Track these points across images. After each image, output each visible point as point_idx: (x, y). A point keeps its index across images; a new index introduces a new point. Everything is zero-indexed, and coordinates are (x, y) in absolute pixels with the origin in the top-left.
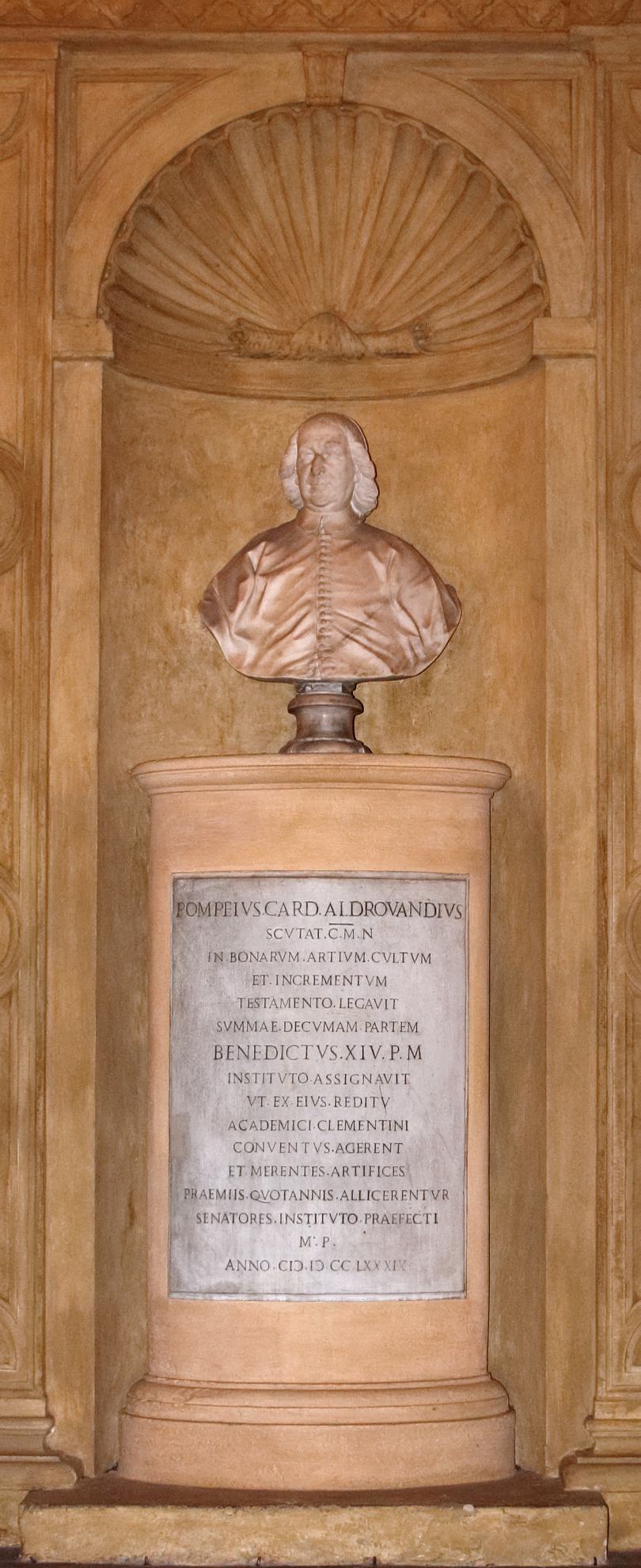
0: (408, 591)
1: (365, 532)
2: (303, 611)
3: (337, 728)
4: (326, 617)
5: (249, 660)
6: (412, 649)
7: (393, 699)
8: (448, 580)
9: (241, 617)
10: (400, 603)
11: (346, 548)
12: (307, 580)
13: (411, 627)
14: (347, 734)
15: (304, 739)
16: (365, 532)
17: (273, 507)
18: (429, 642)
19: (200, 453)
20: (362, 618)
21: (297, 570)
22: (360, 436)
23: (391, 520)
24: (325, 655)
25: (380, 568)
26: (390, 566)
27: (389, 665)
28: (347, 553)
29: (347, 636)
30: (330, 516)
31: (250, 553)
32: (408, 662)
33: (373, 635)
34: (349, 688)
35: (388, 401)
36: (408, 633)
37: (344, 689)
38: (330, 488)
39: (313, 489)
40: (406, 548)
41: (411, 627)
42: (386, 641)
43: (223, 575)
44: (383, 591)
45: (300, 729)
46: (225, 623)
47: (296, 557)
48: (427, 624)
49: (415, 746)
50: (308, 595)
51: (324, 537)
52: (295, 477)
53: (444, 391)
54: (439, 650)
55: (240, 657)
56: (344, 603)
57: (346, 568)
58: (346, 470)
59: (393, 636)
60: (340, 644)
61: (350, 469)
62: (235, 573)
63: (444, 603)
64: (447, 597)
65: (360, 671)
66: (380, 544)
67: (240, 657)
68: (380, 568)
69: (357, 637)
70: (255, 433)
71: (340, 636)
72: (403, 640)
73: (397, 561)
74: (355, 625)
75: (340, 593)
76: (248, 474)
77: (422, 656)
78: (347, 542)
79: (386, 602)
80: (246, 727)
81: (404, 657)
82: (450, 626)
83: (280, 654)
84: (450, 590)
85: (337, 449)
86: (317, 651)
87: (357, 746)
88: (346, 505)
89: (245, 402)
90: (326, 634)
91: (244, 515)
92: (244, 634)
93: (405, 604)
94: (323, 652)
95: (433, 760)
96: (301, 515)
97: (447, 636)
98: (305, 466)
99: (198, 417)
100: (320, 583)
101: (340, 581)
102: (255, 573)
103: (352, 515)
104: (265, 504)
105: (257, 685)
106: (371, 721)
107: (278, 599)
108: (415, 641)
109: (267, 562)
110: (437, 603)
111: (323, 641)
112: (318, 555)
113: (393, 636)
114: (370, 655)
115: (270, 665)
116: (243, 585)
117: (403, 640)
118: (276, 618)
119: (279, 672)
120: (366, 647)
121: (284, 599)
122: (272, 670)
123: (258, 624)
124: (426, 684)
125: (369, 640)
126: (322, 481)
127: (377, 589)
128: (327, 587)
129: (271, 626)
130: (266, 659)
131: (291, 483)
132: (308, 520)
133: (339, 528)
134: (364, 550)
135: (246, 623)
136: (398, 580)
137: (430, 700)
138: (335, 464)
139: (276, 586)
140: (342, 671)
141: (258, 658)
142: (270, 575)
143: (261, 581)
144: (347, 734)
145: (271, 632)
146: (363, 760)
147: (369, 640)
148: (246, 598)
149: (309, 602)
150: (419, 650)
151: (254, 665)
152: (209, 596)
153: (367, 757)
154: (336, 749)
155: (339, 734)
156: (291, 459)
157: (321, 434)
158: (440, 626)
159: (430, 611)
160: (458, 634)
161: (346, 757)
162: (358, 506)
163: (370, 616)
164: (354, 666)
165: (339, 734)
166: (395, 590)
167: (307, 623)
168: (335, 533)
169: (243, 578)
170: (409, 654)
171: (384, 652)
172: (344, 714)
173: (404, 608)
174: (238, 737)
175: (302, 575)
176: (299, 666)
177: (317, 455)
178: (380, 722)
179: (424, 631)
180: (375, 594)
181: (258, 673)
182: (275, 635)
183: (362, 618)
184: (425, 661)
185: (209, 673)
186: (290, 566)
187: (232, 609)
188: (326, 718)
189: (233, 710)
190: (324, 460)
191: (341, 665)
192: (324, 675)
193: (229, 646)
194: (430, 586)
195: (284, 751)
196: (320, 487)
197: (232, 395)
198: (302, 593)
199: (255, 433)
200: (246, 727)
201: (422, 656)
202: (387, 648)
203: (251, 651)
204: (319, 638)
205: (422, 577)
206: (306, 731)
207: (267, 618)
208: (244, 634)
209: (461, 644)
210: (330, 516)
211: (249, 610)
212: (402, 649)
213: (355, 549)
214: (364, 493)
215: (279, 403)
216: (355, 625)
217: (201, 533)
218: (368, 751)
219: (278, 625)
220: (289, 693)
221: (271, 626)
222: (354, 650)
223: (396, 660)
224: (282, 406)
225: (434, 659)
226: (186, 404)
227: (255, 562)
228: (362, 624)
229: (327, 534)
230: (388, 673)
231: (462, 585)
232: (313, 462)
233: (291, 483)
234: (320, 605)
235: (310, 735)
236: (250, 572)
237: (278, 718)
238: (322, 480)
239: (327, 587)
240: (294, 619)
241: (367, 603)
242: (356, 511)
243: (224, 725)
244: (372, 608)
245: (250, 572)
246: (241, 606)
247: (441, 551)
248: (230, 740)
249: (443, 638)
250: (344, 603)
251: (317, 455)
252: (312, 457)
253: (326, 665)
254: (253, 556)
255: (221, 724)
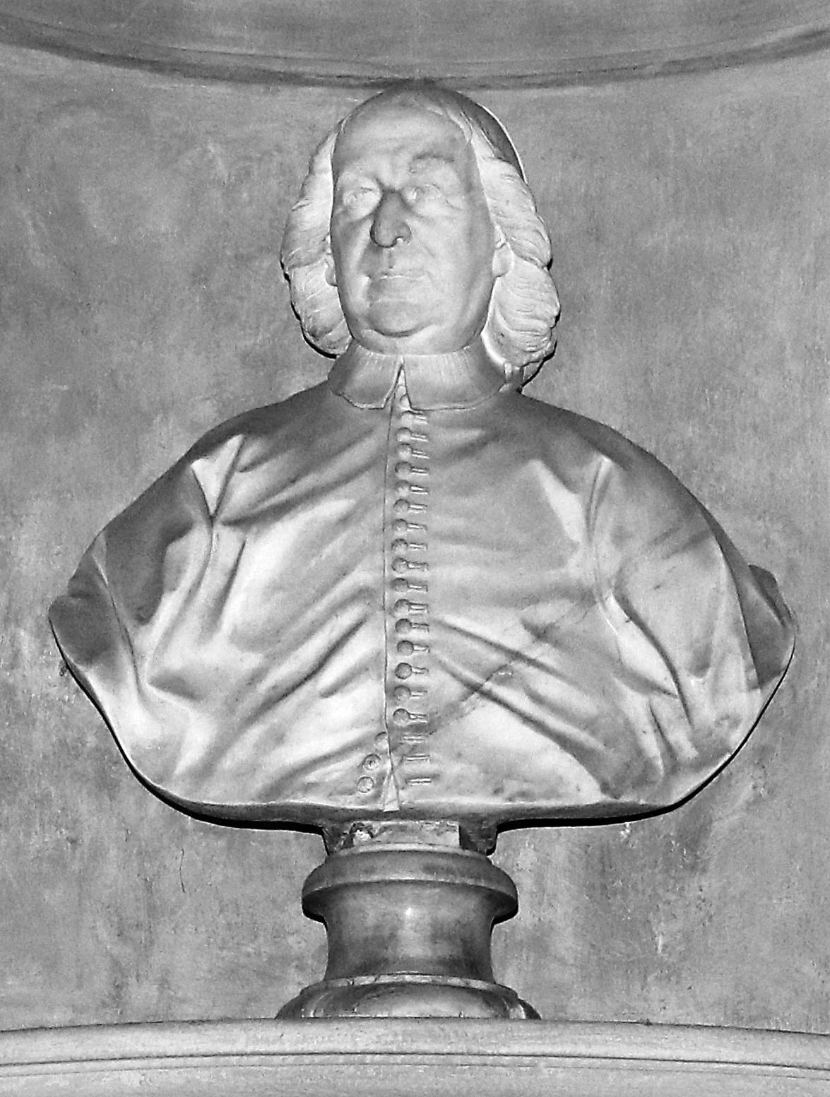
0: (646, 571)
1: (521, 415)
2: (346, 619)
3: (444, 950)
4: (414, 635)
5: (191, 756)
6: (659, 729)
7: (601, 878)
8: (752, 554)
9: (170, 637)
10: (624, 602)
11: (467, 451)
12: (361, 533)
13: (655, 669)
14: (467, 965)
15: (351, 980)
16: (521, 415)
17: (266, 363)
18: (706, 713)
19: (68, 217)
20: (517, 639)
21: (331, 507)
22: (326, 927)
23: (590, 387)
24: (412, 740)
25: (566, 506)
26: (595, 498)
27: (594, 771)
28: (468, 464)
29: (474, 688)
30: (425, 361)
31: (198, 466)
32: (648, 766)
33: (551, 687)
34: (482, 832)
35: (581, 90)
36: (647, 686)
37: (465, 841)
38: (426, 280)
39: (376, 287)
40: (635, 460)
41: (655, 669)
42: (585, 704)
43: (121, 530)
44: (577, 569)
45: (336, 951)
46: (124, 657)
47: (330, 473)
48: (701, 665)
49: (662, 1000)
50: (361, 576)
51: (408, 421)
52: (326, 265)
53: (735, 60)
54: (736, 737)
55: (168, 749)
56: (463, 597)
57: (468, 503)
58: (471, 233)
59: (605, 692)
60: (454, 710)
61: (480, 227)
62: (151, 527)
63: (746, 610)
64: (753, 594)
65: (512, 786)
66: (565, 444)
67: (168, 749)
68: (566, 506)
69: (502, 692)
70: (221, 168)
71: (453, 689)
72: (635, 705)
73: (616, 489)
74: (495, 658)
75: (455, 569)
76: (200, 275)
77: (688, 752)
78: (475, 434)
79: (586, 598)
80: (187, 954)
81: (640, 752)
82: (765, 671)
83: (279, 738)
84: (763, 579)
85: (444, 175)
86: (388, 730)
87: (501, 1001)
88: (469, 337)
89: (189, 89)
90: (412, 680)
91: (194, 376)
92: (177, 685)
93: (639, 605)
94: (406, 731)
95: (700, 1036)
96: (343, 367)
97: (758, 698)
98: (355, 226)
99: (66, 122)
100: (392, 539)
101: (455, 537)
102: (211, 520)
103: (488, 370)
104: (245, 357)
105: (218, 839)
106: (539, 942)
107: (275, 587)
108: (667, 709)
109: (246, 488)
110: (727, 607)
111: (406, 701)
112: (386, 468)
113: (605, 692)
114: (538, 741)
115: (252, 768)
116: (174, 549)
117: (635, 705)
118: (270, 639)
119: (277, 788)
120: (527, 719)
121: (301, 590)
122: (259, 783)
123: (220, 656)
124: (693, 839)
125: (537, 698)
126: (401, 263)
127: (561, 562)
128: (414, 552)
129: (253, 660)
130: (240, 752)
131: (314, 282)
132: (362, 376)
133: (457, 396)
134: (524, 458)
135: (183, 655)
136: (620, 537)
137: (709, 884)
138: (438, 217)
139: (270, 552)
140: (457, 785)
141: (217, 751)
142: (251, 521)
143: (228, 539)
144: (467, 965)
145: (255, 677)
146: (519, 1039)
147: (537, 698)
148: (186, 583)
149: (362, 594)
150: (679, 736)
151: (205, 770)
152: (84, 587)
153: (533, 1028)
154: (443, 1007)
155: (452, 966)
156: (315, 213)
157: (399, 132)
158: (736, 669)
159: (710, 630)
160: (783, 701)
161: (476, 1029)
162: (503, 342)
163: (541, 634)
164: (496, 772)
165: (452, 966)
166: (609, 568)
167: (359, 649)
168: (441, 411)
169: (179, 531)
170: (651, 745)
171: (582, 736)
172: (461, 910)
173: (633, 616)
174: (164, 983)
175: (345, 520)
176: (335, 771)
177: (387, 193)
178: (566, 943)
179: (693, 684)
180: (553, 576)
181: (213, 795)
182: (264, 687)
183: (517, 639)
184: (698, 766)
185: (84, 806)
186: (312, 496)
187: (145, 615)
188: (415, 921)
189: (152, 910)
190: (406, 207)
191: (454, 769)
192: (408, 797)
193: (136, 717)
194: (707, 562)
195: (292, 1012)
196: (398, 279)
197: (156, 67)
198: (344, 572)
199: (221, 168)
200: (187, 954)
201: (688, 752)
202: (590, 725)
203: (196, 731)
204: (393, 691)
205: (684, 535)
206: (354, 959)
207: (246, 640)
208: (177, 685)
209: (792, 728)
210: (425, 361)
211: (194, 620)
212: (629, 730)
213: (493, 452)
214: (523, 305)
215: (285, 92)
216: (495, 658)
217: (68, 427)
218: (532, 1014)
219: (275, 659)
220: (300, 854)
221: (253, 660)
222: (492, 727)
223: (614, 759)
224: (287, 100)
225: (718, 762)
226: (33, 86)
227: (212, 490)
228: (516, 655)
229: (415, 411)
230: (588, 793)
231: (792, 568)
232: (376, 214)
233: (314, 282)
234: (397, 601)
235: (364, 970)
236: (194, 511)
237: (278, 934)
238: (402, 263)
239: (414, 552)
240: (318, 644)
241: (534, 599)
242: (497, 358)
243: (125, 952)
244: (545, 613)
245: (194, 511)
246: (169, 606)
247: (736, 478)
248: (142, 995)
249: (747, 703)
250: (463, 597)
251: (387, 193)
252: (374, 198)
253: (410, 768)
254: (208, 472)
255: (118, 950)
